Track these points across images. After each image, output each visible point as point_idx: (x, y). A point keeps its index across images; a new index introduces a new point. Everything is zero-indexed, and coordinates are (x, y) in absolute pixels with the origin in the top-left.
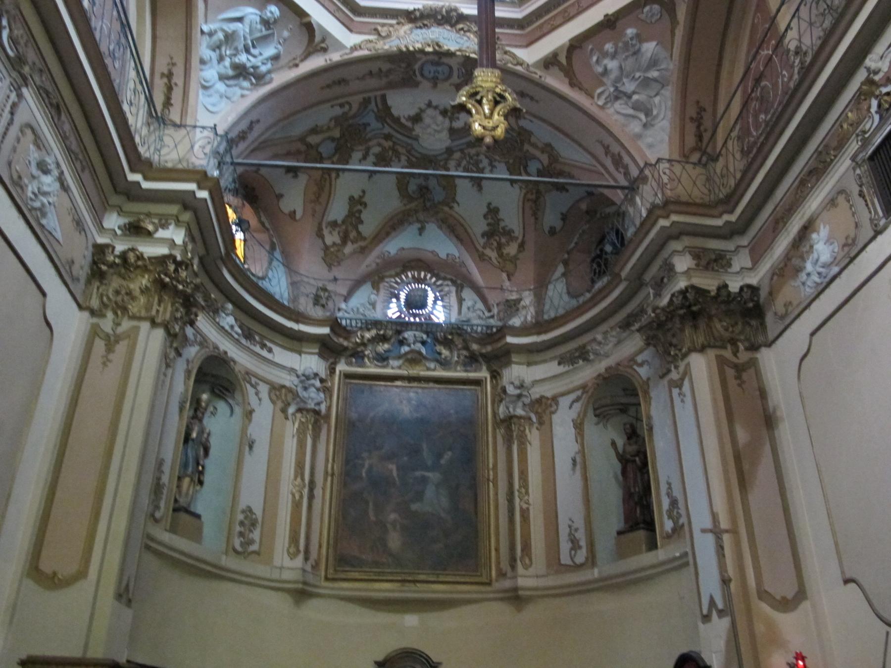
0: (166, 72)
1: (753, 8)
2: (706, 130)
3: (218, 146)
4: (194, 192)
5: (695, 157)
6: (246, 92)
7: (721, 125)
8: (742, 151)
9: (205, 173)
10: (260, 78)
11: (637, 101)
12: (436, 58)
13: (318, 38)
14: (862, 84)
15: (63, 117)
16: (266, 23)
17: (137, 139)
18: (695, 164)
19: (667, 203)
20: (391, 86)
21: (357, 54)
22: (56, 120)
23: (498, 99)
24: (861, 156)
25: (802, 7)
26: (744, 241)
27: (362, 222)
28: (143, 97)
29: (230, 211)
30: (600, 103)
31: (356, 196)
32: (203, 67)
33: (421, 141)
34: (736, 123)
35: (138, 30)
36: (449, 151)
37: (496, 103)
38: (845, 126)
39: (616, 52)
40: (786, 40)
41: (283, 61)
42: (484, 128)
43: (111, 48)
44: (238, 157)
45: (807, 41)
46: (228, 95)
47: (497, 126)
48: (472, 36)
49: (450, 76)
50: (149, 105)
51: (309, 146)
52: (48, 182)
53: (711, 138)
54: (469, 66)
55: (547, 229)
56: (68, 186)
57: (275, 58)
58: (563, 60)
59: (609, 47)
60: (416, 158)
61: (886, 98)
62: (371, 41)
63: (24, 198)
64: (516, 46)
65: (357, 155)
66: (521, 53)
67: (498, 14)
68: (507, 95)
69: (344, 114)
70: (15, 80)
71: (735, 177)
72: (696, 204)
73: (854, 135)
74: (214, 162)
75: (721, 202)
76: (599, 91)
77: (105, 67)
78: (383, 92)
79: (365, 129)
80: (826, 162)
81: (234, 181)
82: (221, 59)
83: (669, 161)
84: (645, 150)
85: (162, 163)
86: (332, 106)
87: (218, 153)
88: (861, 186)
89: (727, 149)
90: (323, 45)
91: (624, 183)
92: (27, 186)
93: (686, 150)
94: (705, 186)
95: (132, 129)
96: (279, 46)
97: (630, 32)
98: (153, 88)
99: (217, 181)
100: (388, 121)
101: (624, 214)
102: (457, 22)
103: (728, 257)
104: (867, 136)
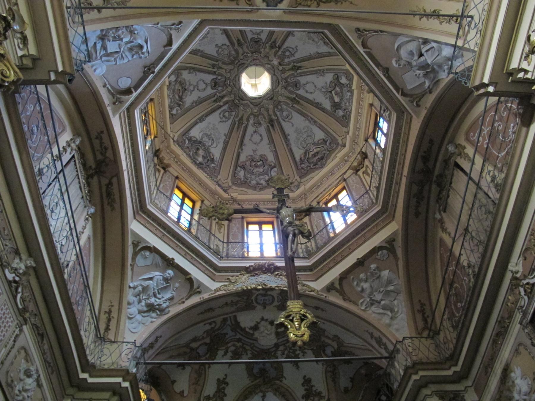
0: (107, 310)
1: (438, 246)
2: (428, 316)
3: (136, 353)
4: (120, 383)
5: (425, 334)
6: (154, 320)
7: (436, 312)
8: (453, 326)
9: (128, 370)
10: (162, 311)
11: (384, 304)
12: (264, 292)
13: (195, 287)
14: (511, 280)
15: (45, 342)
16: (166, 280)
17: (88, 352)
18: (426, 338)
19: (414, 364)
20: (239, 310)
21: (218, 293)
22: (40, 343)
23: (303, 318)
24: (524, 321)
25: (465, 243)
26: (470, 383)
27: (225, 395)
28: (93, 326)
29: (142, 394)
30: (363, 308)
31: (222, 379)
32: (129, 306)
33: (259, 341)
34: (445, 310)
35: (93, 289)
36: (277, 346)
37: (302, 320)
38: (509, 304)
39: (367, 279)
40: (461, 261)
41: (175, 301)
42: (296, 336)
43: (78, 299)
44: (148, 360)
45: (472, 260)
46: (144, 322)
47: (304, 334)
48: (283, 278)
49: (273, 301)
50: (96, 330)
51: (192, 349)
52: (30, 382)
53: (432, 321)
54: (282, 298)
55: (342, 389)
56: (42, 384)
57: (171, 299)
58: (338, 286)
59: (362, 276)
60: (257, 351)
61: (527, 286)
62: (226, 286)
63: (12, 394)
64: (309, 281)
65: (221, 353)
66: (312, 285)
67: (296, 264)
68: (307, 315)
69: (212, 328)
70: (20, 321)
71: (452, 343)
72: (432, 363)
73: (516, 310)
74: (134, 363)
75: (447, 359)
76: (361, 301)
77: (72, 310)
78: (235, 314)
79: (225, 336)
80: (504, 327)
81: (145, 375)
82: (140, 301)
83: (411, 338)
84: (394, 332)
85: (102, 366)
86: (205, 324)
87: (136, 357)
88: (531, 339)
89: (444, 326)
90: (198, 290)
91: (386, 355)
92: (16, 386)
93: (419, 329)
94: (435, 350)
95: (85, 346)
96: (173, 292)
97: (373, 266)
98: (99, 320)
99: (135, 375)
100: (239, 331)
101: (389, 374)
102: (274, 271)
103: (461, 395)
104: (524, 309)
